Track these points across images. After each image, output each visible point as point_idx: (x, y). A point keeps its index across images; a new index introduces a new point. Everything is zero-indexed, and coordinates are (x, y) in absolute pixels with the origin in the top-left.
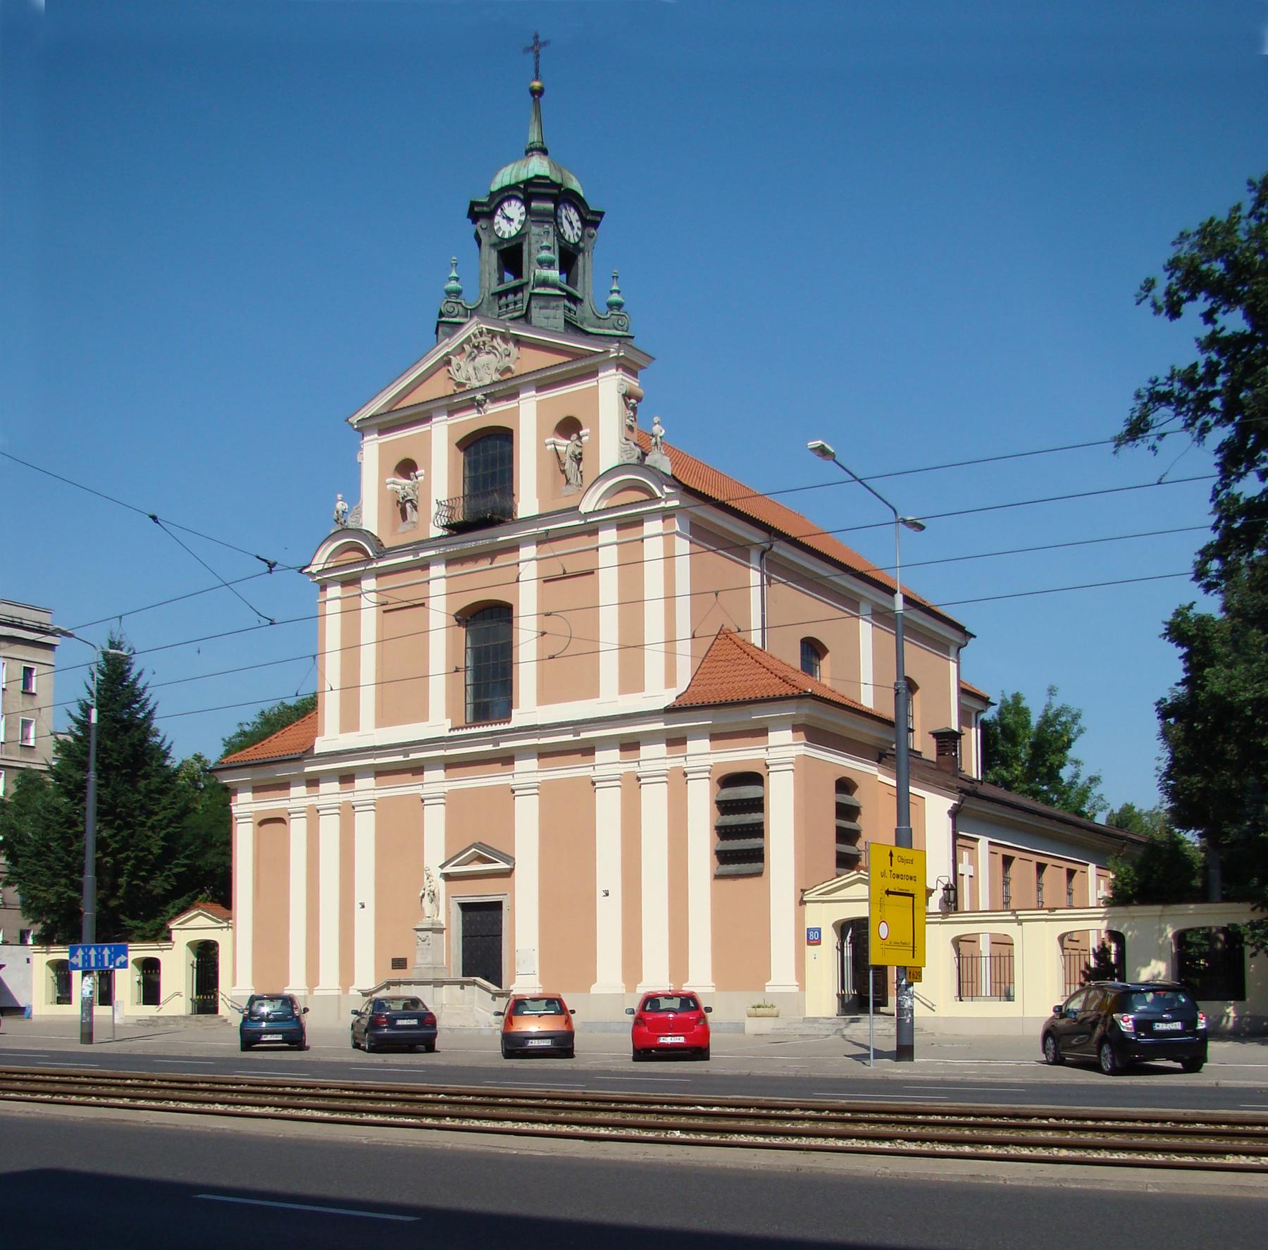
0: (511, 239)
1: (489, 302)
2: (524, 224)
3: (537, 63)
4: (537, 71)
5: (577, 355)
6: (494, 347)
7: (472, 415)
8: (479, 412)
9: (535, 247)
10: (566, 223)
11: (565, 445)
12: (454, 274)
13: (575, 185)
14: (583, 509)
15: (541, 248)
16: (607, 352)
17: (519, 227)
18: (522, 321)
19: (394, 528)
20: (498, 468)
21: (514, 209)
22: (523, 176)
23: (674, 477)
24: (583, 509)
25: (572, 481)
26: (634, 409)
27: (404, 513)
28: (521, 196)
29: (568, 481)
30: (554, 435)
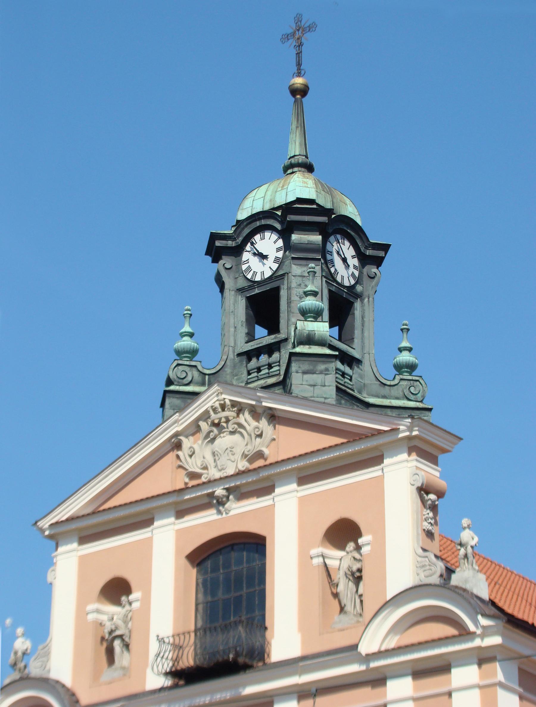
0: (260, 284)
1: (234, 366)
2: (280, 262)
3: (299, 54)
4: (299, 64)
5: (354, 435)
6: (240, 425)
7: (209, 516)
8: (219, 512)
9: (297, 292)
10: (338, 261)
11: (338, 559)
12: (187, 328)
13: (349, 210)
14: (364, 649)
15: (305, 321)
16: (395, 430)
17: (275, 266)
18: (278, 390)
19: (96, 675)
20: (245, 591)
21: (269, 243)
22: (281, 199)
23: (493, 603)
24: (364, 649)
25: (349, 608)
26: (434, 508)
27: (110, 653)
28: (278, 226)
29: (342, 609)
30: (322, 544)
